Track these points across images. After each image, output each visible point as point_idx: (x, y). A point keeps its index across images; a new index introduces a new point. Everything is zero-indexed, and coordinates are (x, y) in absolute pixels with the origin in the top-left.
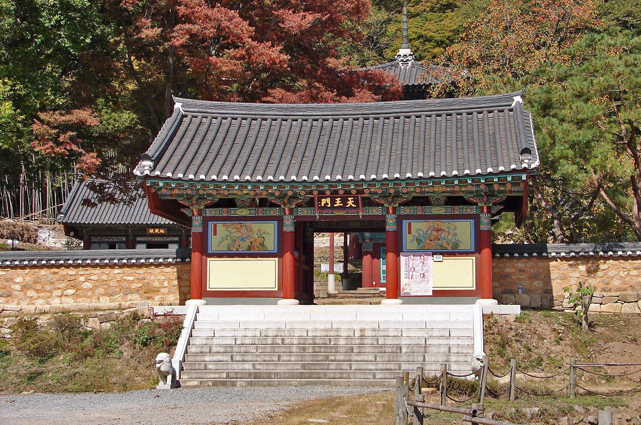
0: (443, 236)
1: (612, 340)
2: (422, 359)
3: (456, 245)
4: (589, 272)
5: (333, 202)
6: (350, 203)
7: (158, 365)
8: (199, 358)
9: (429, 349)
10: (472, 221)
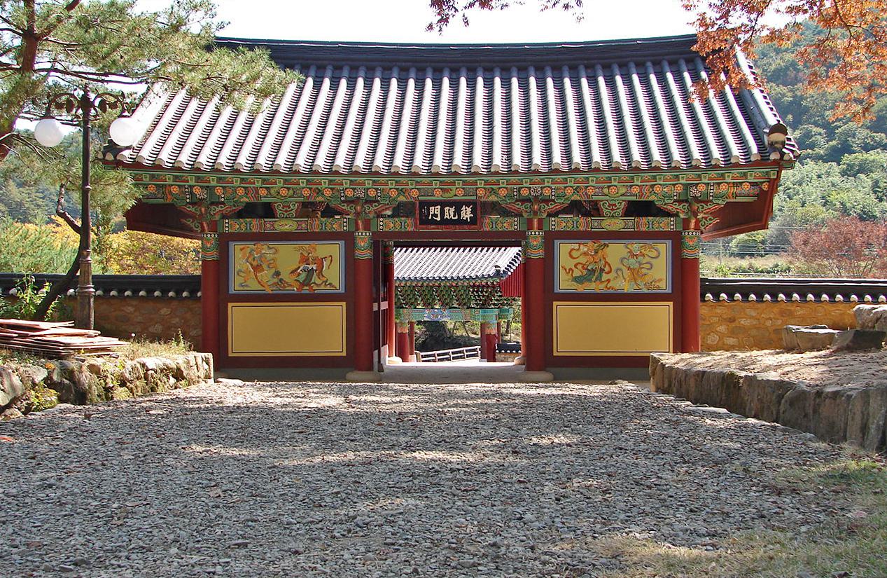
10: (342, 243)
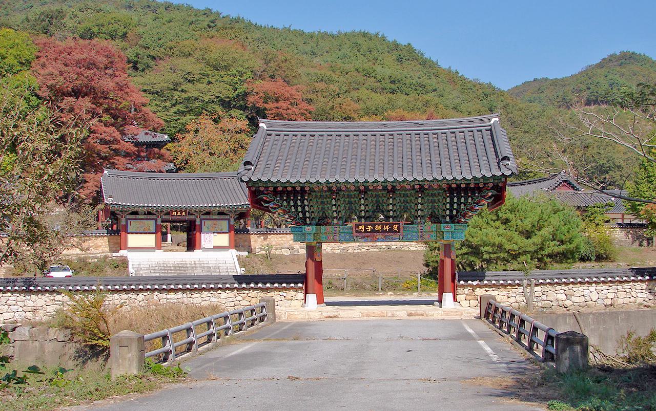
1: (278, 263)
3: (222, 230)
4: (264, 239)
5: (177, 213)
6: (184, 214)
9: (220, 268)
10: (154, 221)
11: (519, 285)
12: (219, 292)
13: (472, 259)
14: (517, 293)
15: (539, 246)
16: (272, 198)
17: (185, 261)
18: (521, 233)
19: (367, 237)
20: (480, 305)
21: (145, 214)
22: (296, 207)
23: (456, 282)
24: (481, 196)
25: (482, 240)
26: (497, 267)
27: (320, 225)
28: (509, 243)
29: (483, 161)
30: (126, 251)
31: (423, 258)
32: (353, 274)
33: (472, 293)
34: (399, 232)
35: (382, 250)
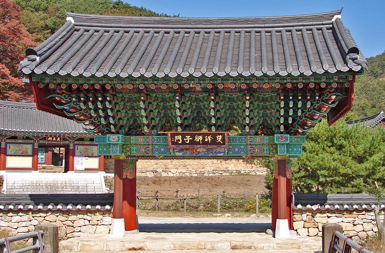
0: (88, 151)
1: (141, 184)
2: (86, 190)
3: (93, 154)
5: (53, 139)
6: (58, 139)
7: (3, 192)
8: (11, 190)
10: (32, 145)
11: (366, 210)
12: (11, 214)
13: (310, 182)
14: (365, 220)
15: (371, 171)
16: (68, 99)
17: (57, 181)
18: (354, 158)
19: (186, 149)
20: (323, 234)
21: (23, 139)
22: (96, 110)
23: (293, 205)
24: (323, 101)
25: (318, 164)
26: (332, 189)
27: (129, 135)
28: (343, 167)
29: (325, 57)
30: (4, 171)
31: (265, 181)
32: (206, 195)
33: (312, 219)
34: (224, 144)
35: (233, 174)
